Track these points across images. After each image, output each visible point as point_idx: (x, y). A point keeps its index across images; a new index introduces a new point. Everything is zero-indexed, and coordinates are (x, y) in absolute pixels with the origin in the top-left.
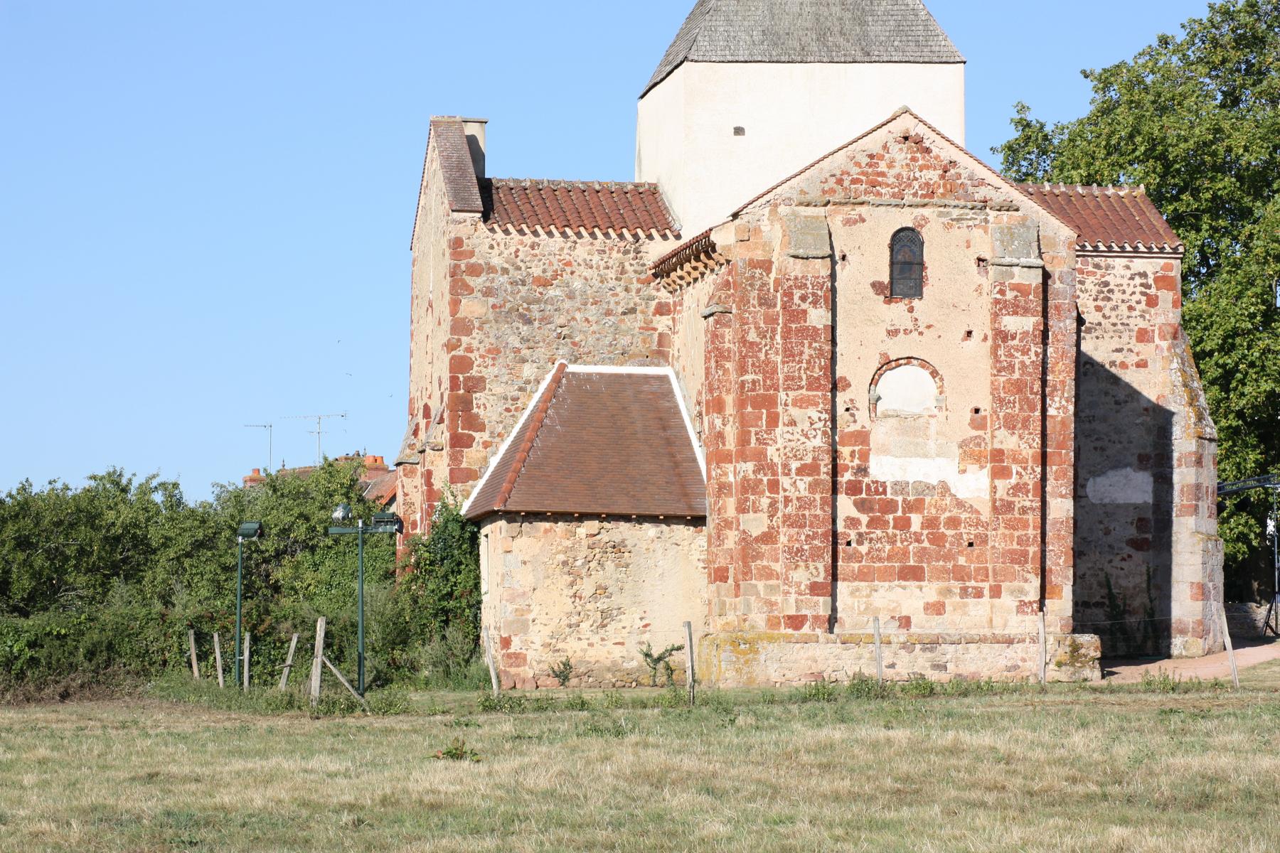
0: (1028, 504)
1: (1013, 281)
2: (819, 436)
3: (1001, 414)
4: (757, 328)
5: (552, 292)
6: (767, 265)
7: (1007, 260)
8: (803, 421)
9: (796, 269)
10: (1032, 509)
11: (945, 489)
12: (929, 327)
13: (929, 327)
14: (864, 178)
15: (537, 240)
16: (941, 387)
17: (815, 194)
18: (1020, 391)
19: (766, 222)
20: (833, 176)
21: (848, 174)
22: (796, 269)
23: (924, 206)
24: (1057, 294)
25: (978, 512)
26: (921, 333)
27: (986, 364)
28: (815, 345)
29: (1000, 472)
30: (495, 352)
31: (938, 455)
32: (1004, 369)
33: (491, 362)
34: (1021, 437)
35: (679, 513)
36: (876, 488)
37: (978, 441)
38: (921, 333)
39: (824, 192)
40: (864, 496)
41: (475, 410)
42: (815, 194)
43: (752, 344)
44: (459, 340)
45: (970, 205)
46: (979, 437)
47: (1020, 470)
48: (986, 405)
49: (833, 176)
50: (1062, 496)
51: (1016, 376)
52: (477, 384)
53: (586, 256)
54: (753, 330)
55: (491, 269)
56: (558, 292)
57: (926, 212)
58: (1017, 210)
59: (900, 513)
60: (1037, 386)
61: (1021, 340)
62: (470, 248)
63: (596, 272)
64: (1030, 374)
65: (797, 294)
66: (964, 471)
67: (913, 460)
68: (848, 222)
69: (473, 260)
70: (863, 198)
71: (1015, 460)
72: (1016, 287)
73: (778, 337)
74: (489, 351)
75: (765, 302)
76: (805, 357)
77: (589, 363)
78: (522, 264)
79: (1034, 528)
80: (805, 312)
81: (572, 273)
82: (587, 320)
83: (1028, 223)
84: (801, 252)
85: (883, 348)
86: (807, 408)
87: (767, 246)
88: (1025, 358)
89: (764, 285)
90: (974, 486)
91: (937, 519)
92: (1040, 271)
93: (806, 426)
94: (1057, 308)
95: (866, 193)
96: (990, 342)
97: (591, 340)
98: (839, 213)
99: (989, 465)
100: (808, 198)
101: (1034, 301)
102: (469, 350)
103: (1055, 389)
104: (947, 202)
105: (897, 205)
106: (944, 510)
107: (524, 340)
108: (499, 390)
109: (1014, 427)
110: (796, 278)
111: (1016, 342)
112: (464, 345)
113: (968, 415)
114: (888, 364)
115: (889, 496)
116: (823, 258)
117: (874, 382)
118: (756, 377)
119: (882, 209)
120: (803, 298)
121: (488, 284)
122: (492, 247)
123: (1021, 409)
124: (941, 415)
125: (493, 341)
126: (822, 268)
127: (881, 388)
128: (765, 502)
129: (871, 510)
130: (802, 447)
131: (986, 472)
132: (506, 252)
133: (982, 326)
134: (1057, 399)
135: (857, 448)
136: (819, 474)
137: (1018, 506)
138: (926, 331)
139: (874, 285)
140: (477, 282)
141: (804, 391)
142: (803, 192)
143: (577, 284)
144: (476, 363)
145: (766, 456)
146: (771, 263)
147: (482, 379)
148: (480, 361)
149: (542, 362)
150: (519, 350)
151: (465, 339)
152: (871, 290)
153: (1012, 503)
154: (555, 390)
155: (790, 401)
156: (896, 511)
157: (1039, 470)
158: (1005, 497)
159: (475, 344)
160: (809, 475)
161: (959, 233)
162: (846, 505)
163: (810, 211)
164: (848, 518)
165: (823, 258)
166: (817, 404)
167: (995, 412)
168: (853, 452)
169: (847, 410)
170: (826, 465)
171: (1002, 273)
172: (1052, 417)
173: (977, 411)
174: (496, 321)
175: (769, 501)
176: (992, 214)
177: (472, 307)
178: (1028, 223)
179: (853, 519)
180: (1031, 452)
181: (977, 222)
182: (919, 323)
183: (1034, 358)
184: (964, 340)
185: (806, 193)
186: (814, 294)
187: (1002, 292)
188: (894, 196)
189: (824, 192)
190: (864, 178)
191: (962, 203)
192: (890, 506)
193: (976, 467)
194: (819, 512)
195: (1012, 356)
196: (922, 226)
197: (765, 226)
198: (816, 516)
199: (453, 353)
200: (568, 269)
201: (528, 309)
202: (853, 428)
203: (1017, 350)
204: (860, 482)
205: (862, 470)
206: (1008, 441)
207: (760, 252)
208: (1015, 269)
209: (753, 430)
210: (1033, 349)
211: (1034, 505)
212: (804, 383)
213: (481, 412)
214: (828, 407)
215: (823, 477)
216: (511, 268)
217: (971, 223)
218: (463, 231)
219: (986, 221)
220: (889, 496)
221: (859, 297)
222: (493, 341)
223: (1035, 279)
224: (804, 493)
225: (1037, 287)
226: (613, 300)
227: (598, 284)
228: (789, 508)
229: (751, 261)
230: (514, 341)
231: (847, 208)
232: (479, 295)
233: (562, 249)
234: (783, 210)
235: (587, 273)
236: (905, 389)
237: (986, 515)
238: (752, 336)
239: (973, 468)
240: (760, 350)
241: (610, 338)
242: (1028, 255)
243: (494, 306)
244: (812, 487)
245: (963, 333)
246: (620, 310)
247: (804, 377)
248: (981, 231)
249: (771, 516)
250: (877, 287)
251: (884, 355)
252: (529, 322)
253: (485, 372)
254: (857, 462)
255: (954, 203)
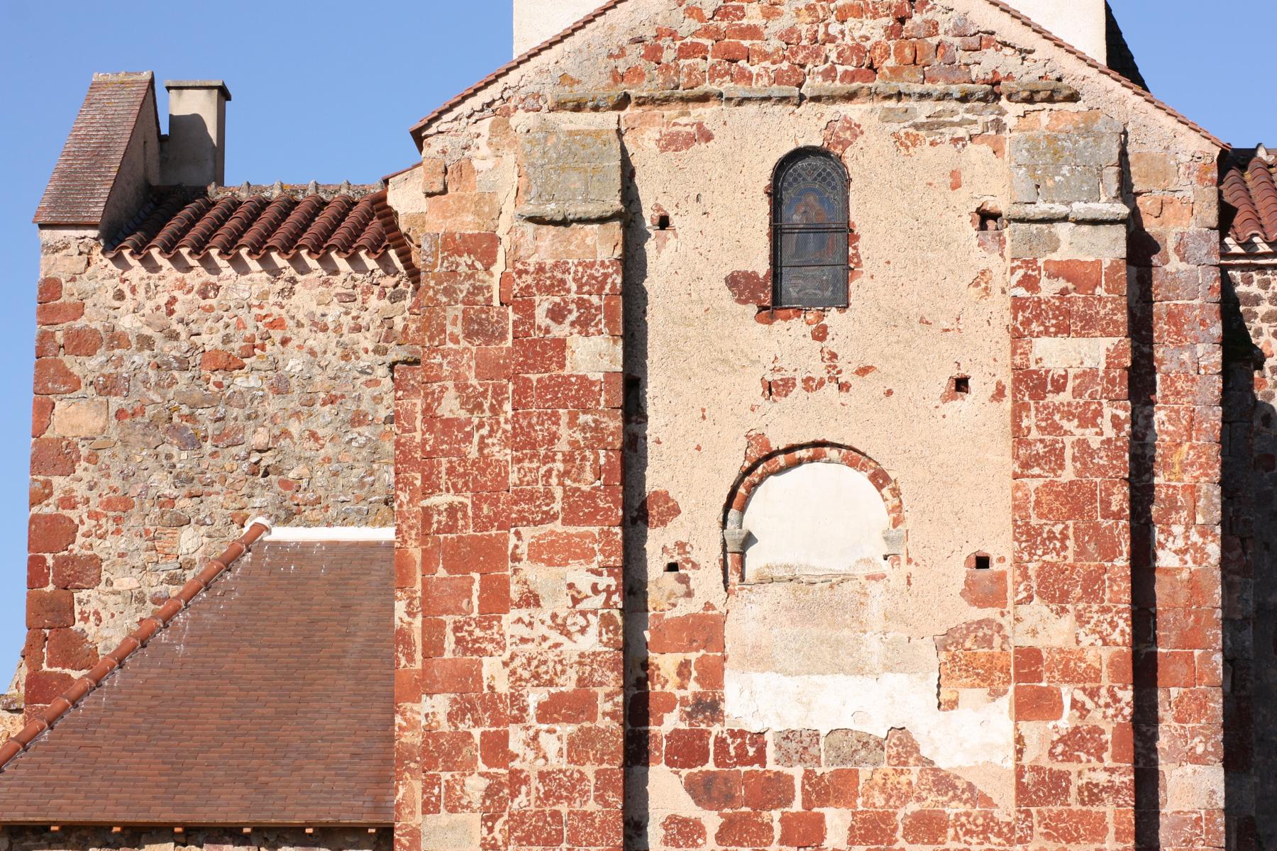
0: (1102, 778)
1: (1055, 257)
2: (593, 630)
3: (1033, 567)
4: (462, 388)
5: (241, 382)
6: (484, 246)
7: (1042, 208)
8: (555, 594)
9: (544, 247)
10: (1112, 789)
11: (903, 745)
12: (863, 371)
13: (863, 371)
14: (708, 42)
15: (213, 279)
16: (898, 508)
17: (595, 83)
18: (1076, 510)
19: (485, 150)
20: (640, 40)
21: (673, 35)
22: (544, 247)
23: (850, 97)
24: (1174, 283)
25: (987, 801)
26: (844, 387)
27: (1001, 457)
28: (583, 418)
29: (1034, 704)
30: (121, 505)
31: (888, 669)
32: (1038, 459)
33: (111, 526)
34: (1080, 619)
35: (347, 819)
36: (741, 747)
37: (984, 632)
38: (844, 387)
39: (617, 77)
40: (711, 766)
41: (79, 625)
42: (595, 83)
43: (448, 423)
44: (48, 484)
45: (956, 90)
46: (988, 622)
47: (1080, 696)
48: (1001, 548)
49: (640, 40)
50: (1197, 760)
51: (1068, 474)
52: (83, 572)
53: (313, 306)
54: (451, 392)
55: (117, 339)
56: (254, 381)
57: (854, 111)
58: (1073, 97)
59: (797, 806)
60: (1119, 498)
61: (1077, 392)
62: (74, 299)
63: (334, 338)
64: (1101, 470)
65: (543, 305)
66: (953, 704)
67: (828, 680)
68: (672, 142)
69: (79, 324)
70: (707, 87)
71: (1068, 675)
72: (1063, 270)
73: (508, 407)
74: (109, 504)
75: (478, 328)
76: (562, 446)
77: (316, 523)
78: (179, 328)
79: (1119, 836)
80: (561, 344)
81: (284, 342)
82: (313, 436)
83: (1099, 126)
84: (550, 209)
85: (755, 423)
86: (564, 563)
87: (485, 204)
88: (1089, 433)
89: (477, 290)
90: (978, 739)
91: (887, 817)
92: (1121, 231)
93: (562, 605)
94: (1173, 317)
95: (714, 74)
96: (1007, 404)
97: (320, 478)
98: (651, 122)
99: (1011, 688)
100: (578, 91)
101: (1111, 302)
102: (68, 502)
103: (1173, 506)
104: (902, 87)
105: (783, 99)
106: (905, 798)
107: (182, 480)
108: (126, 582)
109: (1064, 596)
110: (541, 269)
111: (1065, 397)
112: (57, 494)
113: (960, 572)
114: (765, 461)
115: (771, 766)
116: (602, 220)
117: (735, 500)
118: (457, 499)
119: (751, 108)
120: (557, 314)
121: (109, 369)
122: (120, 296)
123: (1081, 552)
124: (895, 575)
125: (116, 482)
126: (603, 245)
127: (757, 516)
128: (475, 786)
129: (729, 799)
130: (551, 656)
131: (1005, 703)
132: (150, 305)
133: (990, 365)
134: (1178, 529)
135: (693, 656)
136: (592, 718)
137: (1076, 782)
138: (855, 381)
139: (733, 281)
140: (88, 366)
141: (557, 526)
142: (565, 79)
143: (294, 363)
144: (82, 529)
145: (478, 679)
146: (494, 240)
147: (95, 562)
148: (89, 524)
149: (219, 524)
150: (172, 501)
151: (59, 482)
152: (726, 293)
153: (1064, 776)
154: (218, 573)
155: (524, 549)
156: (788, 801)
157: (1127, 695)
158: (1046, 763)
159: (80, 490)
160: (568, 719)
161: (935, 155)
162: (666, 790)
163: (584, 120)
164: (673, 819)
165: (602, 220)
166: (587, 555)
167: (1018, 562)
168: (685, 665)
169: (672, 567)
170: (609, 696)
171: (1029, 240)
172: (1167, 571)
173: (982, 562)
174: (125, 444)
175: (484, 783)
176: (1012, 111)
177: (75, 418)
178: (1099, 126)
179: (685, 822)
180: (1107, 653)
181: (976, 130)
182: (840, 364)
183: (1110, 432)
184: (946, 398)
185: (574, 82)
186: (581, 303)
187: (1029, 282)
188: (778, 78)
189: (617, 77)
190: (708, 42)
191: (940, 87)
192: (776, 791)
193: (983, 692)
194: (592, 806)
195: (1056, 428)
196: (846, 144)
197: (482, 159)
198: (584, 816)
199: (35, 510)
200: (277, 335)
201: (191, 417)
202: (685, 608)
203: (1069, 415)
204: (703, 735)
205: (709, 707)
206: (1049, 629)
207: (469, 218)
208: (1062, 230)
209: (449, 619)
210: (1108, 411)
211: (1117, 779)
212: (557, 506)
213: (90, 628)
214: (616, 560)
215: (603, 723)
216: (158, 337)
217: (961, 132)
218: (62, 266)
219: (999, 126)
220: (771, 766)
221: (699, 310)
222: (116, 482)
223: (1109, 247)
224: (557, 762)
225: (1113, 268)
226: (368, 393)
227: (337, 362)
228: (521, 799)
229: (449, 236)
230: (162, 484)
231: (671, 112)
232: (91, 391)
233: (265, 295)
234: (520, 120)
235: (317, 341)
236: (808, 517)
237: (1006, 808)
238: (450, 406)
239: (972, 696)
240: (469, 437)
241: (360, 471)
242: (1094, 196)
243: (120, 414)
244: (577, 749)
245: (943, 382)
246: (383, 413)
247: (558, 493)
248: (986, 149)
249: (489, 819)
250: (740, 284)
251: (756, 439)
252: (194, 442)
253: (101, 548)
254: (693, 687)
255: (918, 88)
